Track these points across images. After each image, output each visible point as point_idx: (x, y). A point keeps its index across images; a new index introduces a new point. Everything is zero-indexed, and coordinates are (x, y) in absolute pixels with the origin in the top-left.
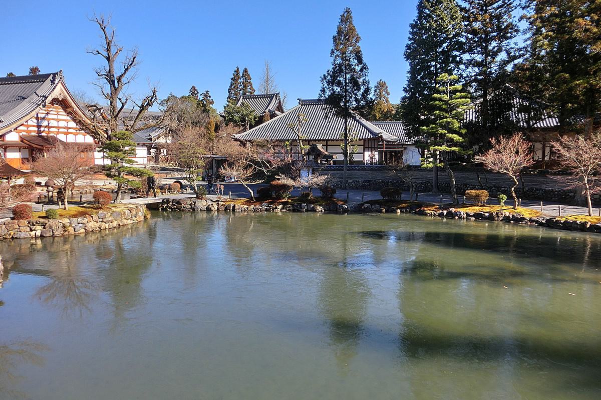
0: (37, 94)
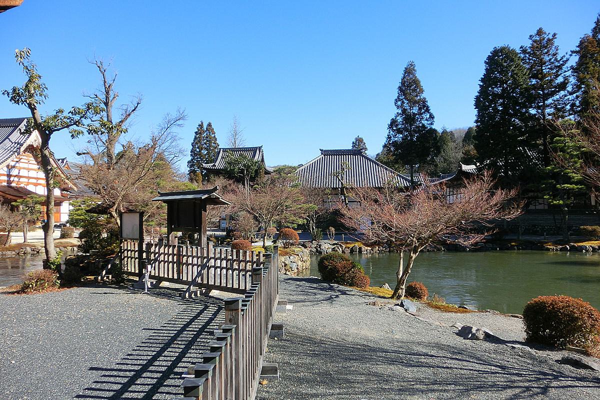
0: (10, 141)
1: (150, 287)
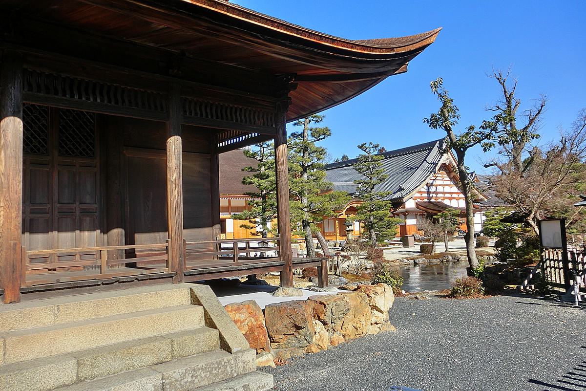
1: (580, 300)
